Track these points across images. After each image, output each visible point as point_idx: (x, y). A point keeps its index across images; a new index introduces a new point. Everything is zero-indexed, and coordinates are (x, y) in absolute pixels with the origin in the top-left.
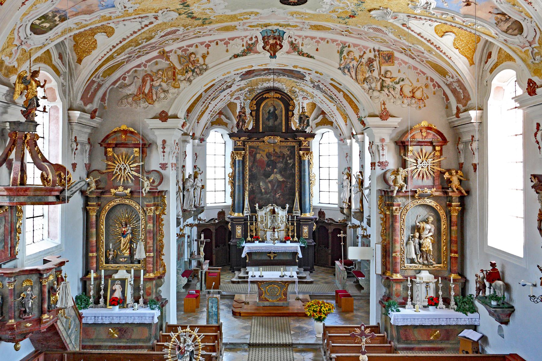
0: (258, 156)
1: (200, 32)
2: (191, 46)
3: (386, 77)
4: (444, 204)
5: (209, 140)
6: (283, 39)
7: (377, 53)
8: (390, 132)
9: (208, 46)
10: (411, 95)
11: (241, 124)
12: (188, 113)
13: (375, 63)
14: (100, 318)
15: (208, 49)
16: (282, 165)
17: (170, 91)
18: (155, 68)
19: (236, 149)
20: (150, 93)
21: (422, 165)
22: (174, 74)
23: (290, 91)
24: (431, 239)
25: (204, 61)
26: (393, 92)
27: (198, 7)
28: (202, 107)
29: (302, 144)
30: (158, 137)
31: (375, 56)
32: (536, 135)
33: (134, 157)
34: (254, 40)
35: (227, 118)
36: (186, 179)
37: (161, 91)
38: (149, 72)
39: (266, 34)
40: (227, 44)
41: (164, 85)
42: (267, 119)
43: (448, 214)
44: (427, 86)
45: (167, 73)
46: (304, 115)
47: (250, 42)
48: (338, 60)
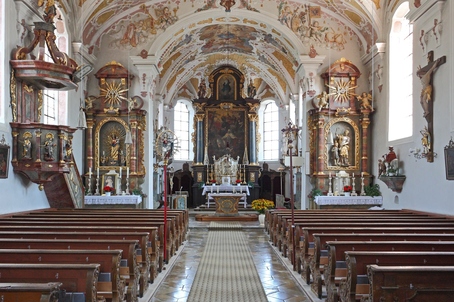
0: (215, 119)
3: (314, 26)
4: (358, 121)
7: (307, 8)
8: (317, 67)
10: (333, 40)
11: (202, 93)
12: (160, 78)
13: (306, 16)
14: (97, 200)
15: (178, 4)
16: (234, 126)
17: (149, 37)
18: (137, 20)
19: (198, 113)
21: (340, 89)
22: (152, 23)
23: (241, 68)
24: (347, 147)
26: (319, 38)
28: (171, 73)
29: (251, 108)
30: (140, 71)
31: (306, 11)
32: (420, 40)
33: (122, 86)
35: (190, 92)
36: (159, 130)
38: (133, 23)
41: (144, 32)
42: (222, 90)
43: (361, 128)
44: (345, 34)
46: (252, 86)
48: (278, 13)
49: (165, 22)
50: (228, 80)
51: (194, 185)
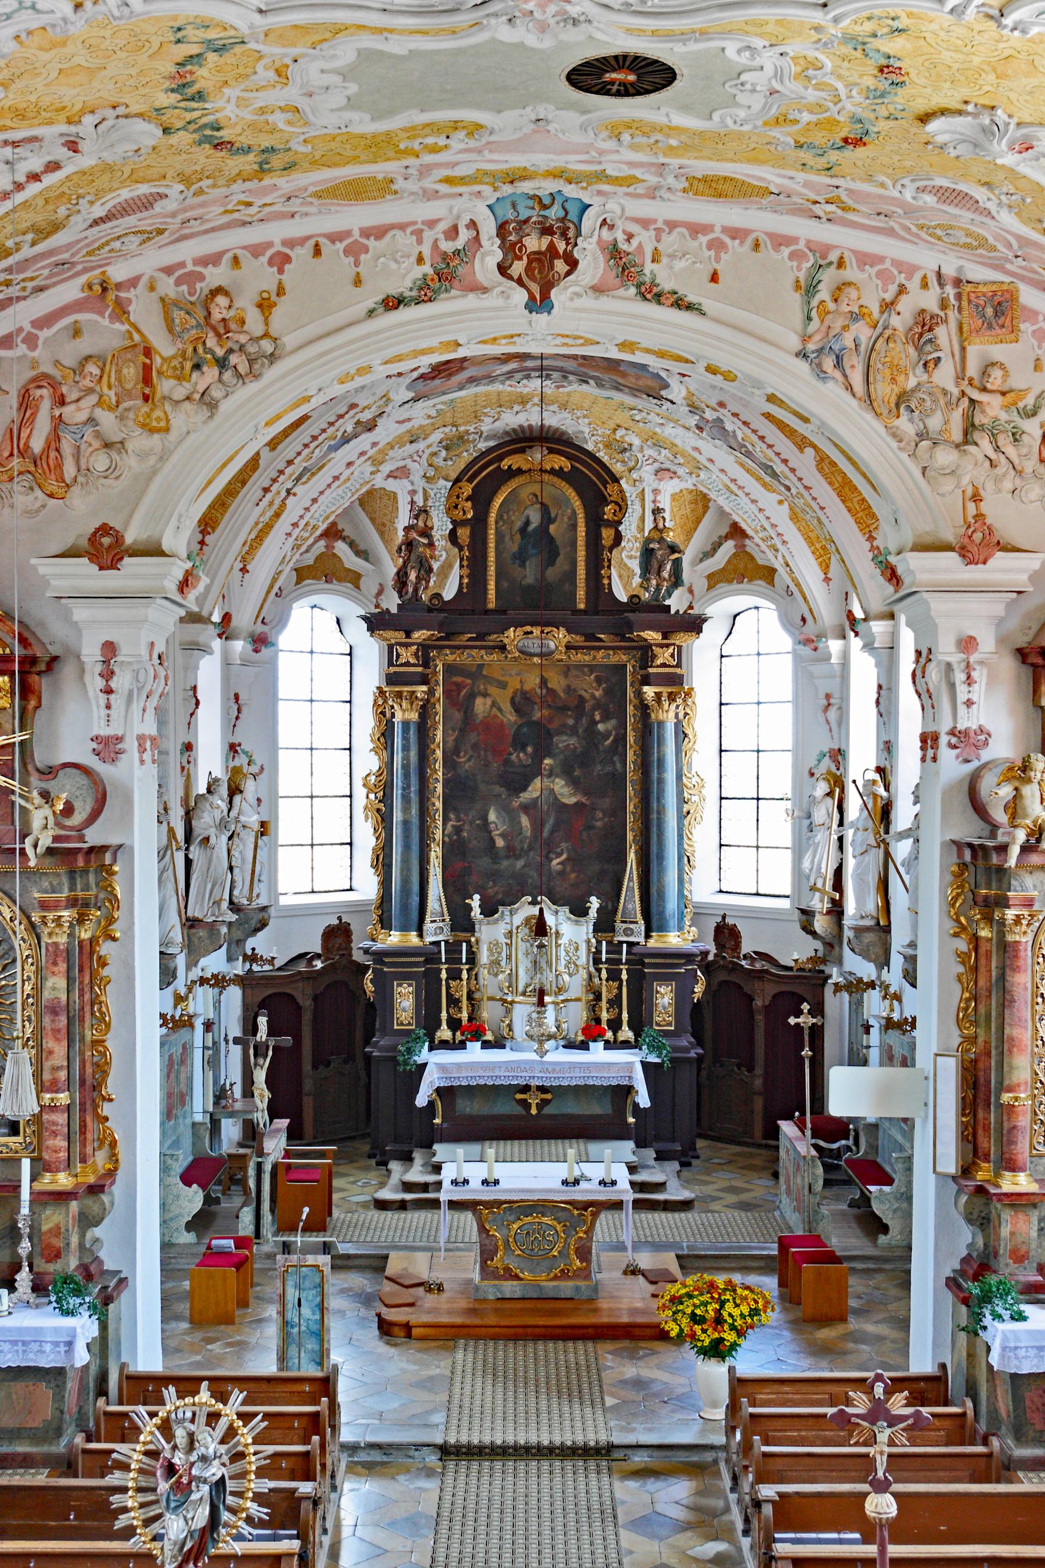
0: (481, 706)
1: (249, 204)
2: (213, 259)
3: (984, 389)
5: (285, 639)
6: (578, 234)
7: (950, 291)
8: (999, 610)
9: (281, 261)
11: (413, 576)
12: (204, 532)
13: (941, 333)
15: (281, 271)
16: (573, 741)
17: (129, 446)
18: (71, 352)
20: (53, 454)
22: (147, 369)
25: (267, 324)
26: (1011, 451)
27: (241, 102)
29: (654, 657)
31: (944, 304)
34: (465, 235)
36: (200, 797)
37: (96, 444)
38: (47, 368)
39: (510, 215)
40: (355, 251)
41: (107, 419)
42: (514, 557)
45: (119, 371)
46: (661, 540)
47: (447, 246)
49: (216, 371)
50: (545, 509)
51: (379, 1046)
